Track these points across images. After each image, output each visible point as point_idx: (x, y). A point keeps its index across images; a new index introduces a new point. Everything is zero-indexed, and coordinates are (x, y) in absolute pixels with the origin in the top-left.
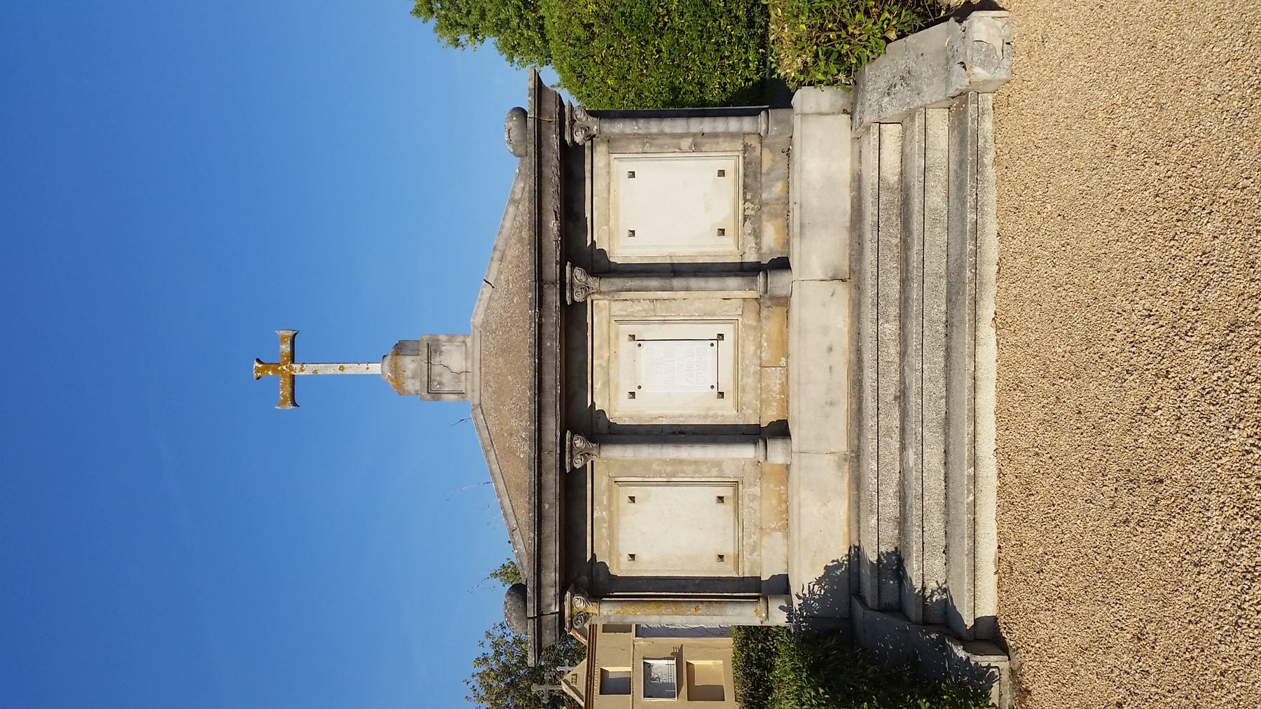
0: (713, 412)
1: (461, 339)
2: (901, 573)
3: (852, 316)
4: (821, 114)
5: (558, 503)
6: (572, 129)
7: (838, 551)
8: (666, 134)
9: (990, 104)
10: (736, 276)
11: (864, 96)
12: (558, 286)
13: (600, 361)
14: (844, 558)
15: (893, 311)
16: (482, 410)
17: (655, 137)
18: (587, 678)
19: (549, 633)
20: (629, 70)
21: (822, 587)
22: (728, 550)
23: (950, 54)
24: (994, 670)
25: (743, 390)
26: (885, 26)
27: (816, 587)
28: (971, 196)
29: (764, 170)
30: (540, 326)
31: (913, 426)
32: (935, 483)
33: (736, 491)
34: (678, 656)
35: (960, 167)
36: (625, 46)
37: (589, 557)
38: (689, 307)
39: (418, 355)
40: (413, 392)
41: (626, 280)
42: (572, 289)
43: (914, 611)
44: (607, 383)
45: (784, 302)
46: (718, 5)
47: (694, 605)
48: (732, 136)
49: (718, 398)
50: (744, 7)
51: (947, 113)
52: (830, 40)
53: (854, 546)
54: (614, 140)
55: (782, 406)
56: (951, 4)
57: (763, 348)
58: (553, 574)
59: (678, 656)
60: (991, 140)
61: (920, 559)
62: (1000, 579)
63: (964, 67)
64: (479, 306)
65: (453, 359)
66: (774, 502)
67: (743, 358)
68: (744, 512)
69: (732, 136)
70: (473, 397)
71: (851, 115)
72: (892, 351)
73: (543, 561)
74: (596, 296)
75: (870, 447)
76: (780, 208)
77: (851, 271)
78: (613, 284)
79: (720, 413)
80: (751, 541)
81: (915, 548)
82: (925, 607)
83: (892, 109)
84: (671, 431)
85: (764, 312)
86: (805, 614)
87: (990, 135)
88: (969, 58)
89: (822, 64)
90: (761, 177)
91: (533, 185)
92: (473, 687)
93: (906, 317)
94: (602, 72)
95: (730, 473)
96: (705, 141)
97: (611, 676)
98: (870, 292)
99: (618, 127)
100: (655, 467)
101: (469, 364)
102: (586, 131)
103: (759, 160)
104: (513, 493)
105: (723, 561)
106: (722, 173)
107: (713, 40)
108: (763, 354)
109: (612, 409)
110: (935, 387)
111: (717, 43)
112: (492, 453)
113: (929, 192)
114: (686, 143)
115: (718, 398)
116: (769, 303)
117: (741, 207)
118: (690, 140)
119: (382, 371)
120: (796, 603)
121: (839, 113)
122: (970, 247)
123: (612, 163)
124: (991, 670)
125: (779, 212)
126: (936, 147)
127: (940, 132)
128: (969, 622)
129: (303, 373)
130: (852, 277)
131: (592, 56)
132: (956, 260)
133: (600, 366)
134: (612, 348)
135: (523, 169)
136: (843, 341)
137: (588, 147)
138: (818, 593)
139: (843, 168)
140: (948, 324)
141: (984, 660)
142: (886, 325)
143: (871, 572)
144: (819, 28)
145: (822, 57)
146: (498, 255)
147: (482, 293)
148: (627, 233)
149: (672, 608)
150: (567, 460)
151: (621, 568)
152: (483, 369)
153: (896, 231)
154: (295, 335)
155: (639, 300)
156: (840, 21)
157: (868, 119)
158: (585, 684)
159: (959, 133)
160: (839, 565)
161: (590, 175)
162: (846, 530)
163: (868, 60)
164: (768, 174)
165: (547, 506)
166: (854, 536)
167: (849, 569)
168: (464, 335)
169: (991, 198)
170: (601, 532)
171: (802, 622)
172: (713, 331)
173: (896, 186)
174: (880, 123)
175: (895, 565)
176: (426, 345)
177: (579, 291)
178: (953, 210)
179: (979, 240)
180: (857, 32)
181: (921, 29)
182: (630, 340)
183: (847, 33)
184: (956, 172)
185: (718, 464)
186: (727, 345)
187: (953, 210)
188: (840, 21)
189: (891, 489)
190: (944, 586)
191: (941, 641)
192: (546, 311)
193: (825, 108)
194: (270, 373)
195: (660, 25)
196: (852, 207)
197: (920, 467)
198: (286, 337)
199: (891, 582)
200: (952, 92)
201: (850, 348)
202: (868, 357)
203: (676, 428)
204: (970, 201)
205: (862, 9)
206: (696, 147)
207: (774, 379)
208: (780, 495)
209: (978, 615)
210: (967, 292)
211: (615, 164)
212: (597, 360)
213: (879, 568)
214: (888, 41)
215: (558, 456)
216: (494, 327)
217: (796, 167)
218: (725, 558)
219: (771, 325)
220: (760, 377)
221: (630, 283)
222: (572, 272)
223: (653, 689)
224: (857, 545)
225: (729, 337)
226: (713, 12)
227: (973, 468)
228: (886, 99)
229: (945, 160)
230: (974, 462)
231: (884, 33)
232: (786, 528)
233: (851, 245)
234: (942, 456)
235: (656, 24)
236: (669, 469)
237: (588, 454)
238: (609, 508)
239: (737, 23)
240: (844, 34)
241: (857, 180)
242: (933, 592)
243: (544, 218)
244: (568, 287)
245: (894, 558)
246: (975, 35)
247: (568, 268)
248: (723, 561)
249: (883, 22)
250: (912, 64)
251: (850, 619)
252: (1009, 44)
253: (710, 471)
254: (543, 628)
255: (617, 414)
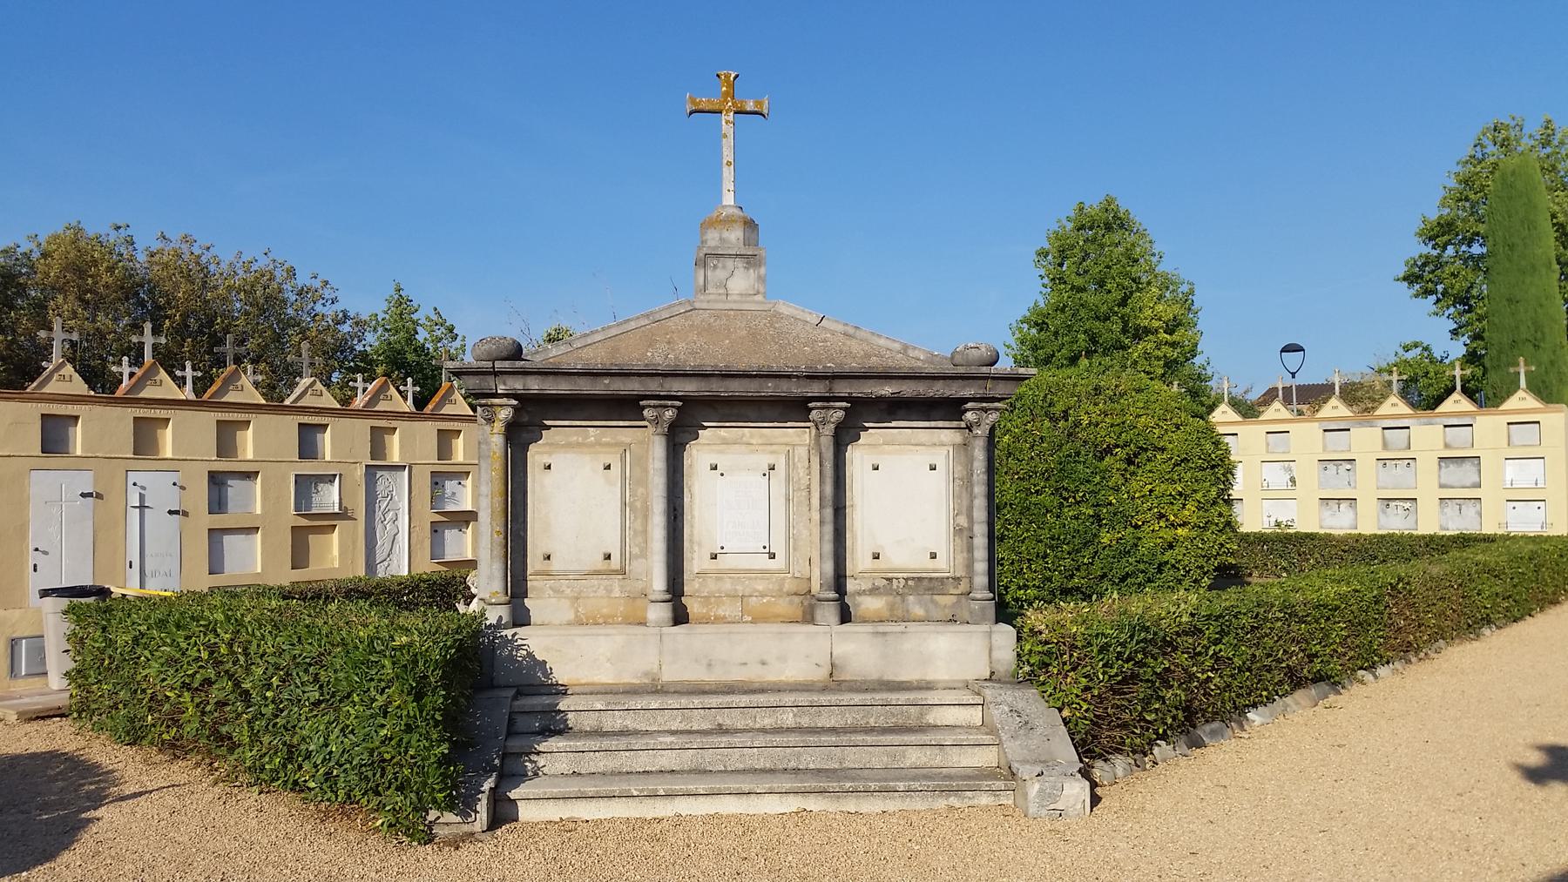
0: (696, 548)
1: (762, 290)
2: (547, 734)
3: (796, 684)
4: (990, 650)
5: (609, 392)
6: (978, 409)
7: (560, 675)
8: (972, 501)
9: (1005, 802)
10: (835, 570)
11: (1009, 689)
12: (827, 395)
13: (748, 435)
14: (554, 680)
15: (805, 721)
16: (689, 311)
17: (969, 489)
18: (318, 408)
19: (476, 383)
20: (1018, 459)
21: (524, 658)
22: (556, 565)
23: (1050, 764)
24: (473, 817)
25: (718, 579)
26: (1074, 706)
27: (525, 652)
28: (920, 786)
29: (936, 597)
30: (789, 377)
31: (698, 741)
32: (642, 761)
33: (616, 572)
34: (344, 515)
35: (945, 776)
36: (1044, 455)
37: (548, 423)
38: (802, 524)
39: (745, 245)
40: (704, 238)
41: (832, 462)
42: (823, 408)
43: (515, 744)
44: (725, 442)
45: (809, 617)
46: (1085, 556)
47: (502, 530)
48: (970, 566)
49: (711, 554)
50: (1083, 584)
51: (993, 765)
52: (1062, 655)
53: (567, 690)
54: (966, 450)
55: (703, 618)
56: (1094, 770)
57: (760, 598)
58: (537, 388)
59: (344, 515)
60: (970, 803)
61: (568, 750)
62: (556, 823)
63: (1039, 775)
64: (797, 309)
65: (741, 281)
66: (605, 611)
67: (750, 579)
68: (594, 581)
69: (970, 566)
70: (702, 301)
71: (990, 680)
72: (767, 721)
73: (551, 377)
74: (814, 431)
75: (672, 702)
76: (899, 613)
77: (840, 682)
78: (828, 449)
79: (696, 555)
80: (564, 588)
81: (580, 744)
82: (520, 755)
83: (997, 714)
84: (677, 508)
85: (797, 599)
86: (497, 641)
87: (975, 802)
88: (1047, 779)
89: (1040, 648)
90: (929, 594)
91: (927, 371)
92: (256, 261)
93: (801, 732)
94: (1016, 430)
95: (635, 567)
96: (965, 539)
97: (319, 436)
98: (824, 699)
99: (979, 455)
100: (641, 490)
101: (735, 298)
102: (977, 423)
103: (945, 592)
104: (609, 343)
105: (545, 559)
106: (933, 556)
107: (1048, 551)
108: (754, 598)
109: (699, 447)
110: (735, 760)
111: (1046, 556)
112: (647, 322)
113: (920, 749)
114: (963, 521)
115: (711, 554)
116: (806, 603)
117: (900, 575)
118: (966, 525)
119: (726, 206)
120: (509, 633)
121: (991, 667)
122: (873, 785)
123: (946, 447)
124: (473, 814)
125: (895, 612)
126: (962, 755)
127: (976, 759)
128: (513, 795)
129: (724, 123)
130: (835, 682)
131: (1033, 420)
132: (859, 775)
133: (743, 435)
134: (761, 448)
135: (938, 359)
136: (771, 676)
137: (960, 424)
138: (519, 655)
139: (939, 672)
140: (796, 770)
141: (482, 806)
142: (791, 715)
143: (548, 704)
144: (1073, 644)
145: (1046, 648)
146: (851, 331)
147: (810, 313)
148: (876, 462)
149: (499, 507)
150: (652, 402)
151: (536, 455)
152: (732, 313)
153: (882, 722)
154: (764, 116)
155: (809, 474)
156: (1080, 664)
157: (988, 693)
158: (312, 405)
159: (977, 775)
160: (547, 675)
161: (933, 426)
162: (583, 681)
163: (1043, 692)
164: (932, 601)
165: (607, 382)
166: (577, 689)
167: (543, 685)
168: (765, 293)
169: (918, 804)
170: (574, 436)
171: (488, 638)
172: (779, 548)
173: (924, 721)
174: (983, 705)
175: (555, 726)
176: (756, 253)
177: (822, 416)
178: (905, 771)
179: (879, 794)
180: (1069, 680)
181: (1073, 739)
182: (769, 465)
183: (1068, 671)
184: (941, 773)
185: (644, 553)
186: (763, 562)
187: (905, 771)
188: (1080, 664)
189: (630, 722)
190: (541, 773)
191: (493, 769)
192: (802, 382)
193: (996, 654)
194: (724, 89)
195: (1065, 494)
196: (903, 682)
197: (659, 747)
198: (762, 107)
199: (537, 725)
200: (1015, 765)
201: (764, 682)
202: (761, 699)
203: (680, 511)
204: (916, 785)
205: (1090, 684)
206: (958, 531)
207: (729, 609)
208: (613, 617)
209: (519, 803)
210: (831, 785)
211: (944, 451)
212: (750, 432)
213: (553, 711)
214: (1060, 710)
215: (658, 393)
216: (777, 325)
217: (941, 628)
218: (547, 561)
219: (784, 606)
220: (732, 596)
221: (829, 466)
222: (840, 408)
223: (305, 485)
224: (569, 692)
225: (772, 565)
226: (1078, 551)
227: (664, 794)
228: (1007, 709)
229: (950, 764)
230: (669, 795)
231: (1068, 705)
232: (579, 622)
233: (865, 681)
234: (668, 769)
235: (1066, 489)
236: (638, 504)
237: (657, 423)
238: (598, 443)
239: (1066, 577)
240: (1067, 667)
241: (928, 686)
242: (535, 762)
243: (894, 381)
244: (826, 404)
245: (562, 726)
246: (1068, 784)
247: (844, 404)
248: (545, 559)
249: (1078, 704)
250: (1039, 730)
251: (492, 686)
252: (1061, 815)
253: (637, 546)
254: (482, 377)
255: (694, 452)
